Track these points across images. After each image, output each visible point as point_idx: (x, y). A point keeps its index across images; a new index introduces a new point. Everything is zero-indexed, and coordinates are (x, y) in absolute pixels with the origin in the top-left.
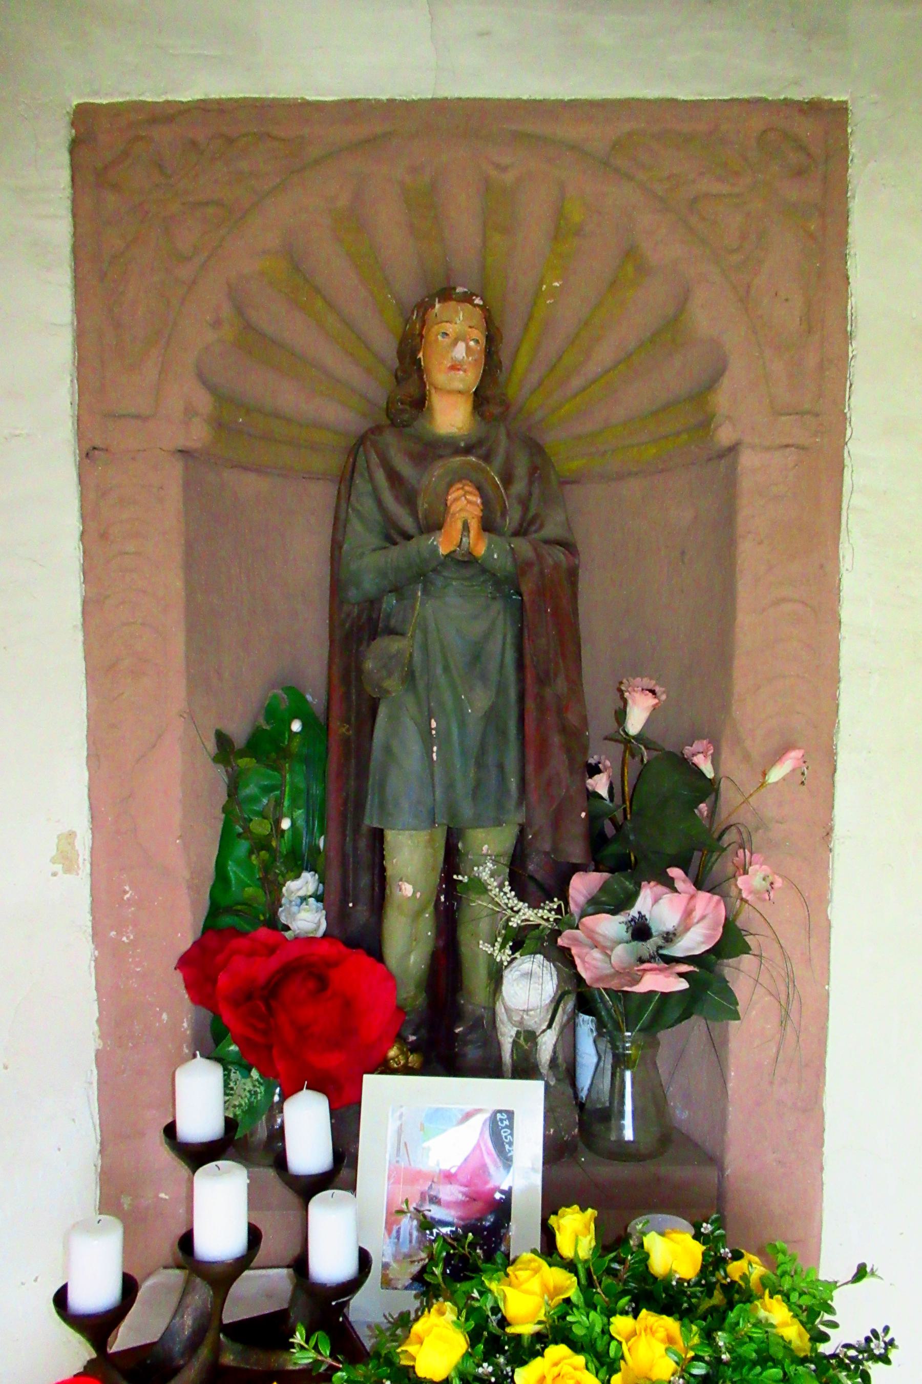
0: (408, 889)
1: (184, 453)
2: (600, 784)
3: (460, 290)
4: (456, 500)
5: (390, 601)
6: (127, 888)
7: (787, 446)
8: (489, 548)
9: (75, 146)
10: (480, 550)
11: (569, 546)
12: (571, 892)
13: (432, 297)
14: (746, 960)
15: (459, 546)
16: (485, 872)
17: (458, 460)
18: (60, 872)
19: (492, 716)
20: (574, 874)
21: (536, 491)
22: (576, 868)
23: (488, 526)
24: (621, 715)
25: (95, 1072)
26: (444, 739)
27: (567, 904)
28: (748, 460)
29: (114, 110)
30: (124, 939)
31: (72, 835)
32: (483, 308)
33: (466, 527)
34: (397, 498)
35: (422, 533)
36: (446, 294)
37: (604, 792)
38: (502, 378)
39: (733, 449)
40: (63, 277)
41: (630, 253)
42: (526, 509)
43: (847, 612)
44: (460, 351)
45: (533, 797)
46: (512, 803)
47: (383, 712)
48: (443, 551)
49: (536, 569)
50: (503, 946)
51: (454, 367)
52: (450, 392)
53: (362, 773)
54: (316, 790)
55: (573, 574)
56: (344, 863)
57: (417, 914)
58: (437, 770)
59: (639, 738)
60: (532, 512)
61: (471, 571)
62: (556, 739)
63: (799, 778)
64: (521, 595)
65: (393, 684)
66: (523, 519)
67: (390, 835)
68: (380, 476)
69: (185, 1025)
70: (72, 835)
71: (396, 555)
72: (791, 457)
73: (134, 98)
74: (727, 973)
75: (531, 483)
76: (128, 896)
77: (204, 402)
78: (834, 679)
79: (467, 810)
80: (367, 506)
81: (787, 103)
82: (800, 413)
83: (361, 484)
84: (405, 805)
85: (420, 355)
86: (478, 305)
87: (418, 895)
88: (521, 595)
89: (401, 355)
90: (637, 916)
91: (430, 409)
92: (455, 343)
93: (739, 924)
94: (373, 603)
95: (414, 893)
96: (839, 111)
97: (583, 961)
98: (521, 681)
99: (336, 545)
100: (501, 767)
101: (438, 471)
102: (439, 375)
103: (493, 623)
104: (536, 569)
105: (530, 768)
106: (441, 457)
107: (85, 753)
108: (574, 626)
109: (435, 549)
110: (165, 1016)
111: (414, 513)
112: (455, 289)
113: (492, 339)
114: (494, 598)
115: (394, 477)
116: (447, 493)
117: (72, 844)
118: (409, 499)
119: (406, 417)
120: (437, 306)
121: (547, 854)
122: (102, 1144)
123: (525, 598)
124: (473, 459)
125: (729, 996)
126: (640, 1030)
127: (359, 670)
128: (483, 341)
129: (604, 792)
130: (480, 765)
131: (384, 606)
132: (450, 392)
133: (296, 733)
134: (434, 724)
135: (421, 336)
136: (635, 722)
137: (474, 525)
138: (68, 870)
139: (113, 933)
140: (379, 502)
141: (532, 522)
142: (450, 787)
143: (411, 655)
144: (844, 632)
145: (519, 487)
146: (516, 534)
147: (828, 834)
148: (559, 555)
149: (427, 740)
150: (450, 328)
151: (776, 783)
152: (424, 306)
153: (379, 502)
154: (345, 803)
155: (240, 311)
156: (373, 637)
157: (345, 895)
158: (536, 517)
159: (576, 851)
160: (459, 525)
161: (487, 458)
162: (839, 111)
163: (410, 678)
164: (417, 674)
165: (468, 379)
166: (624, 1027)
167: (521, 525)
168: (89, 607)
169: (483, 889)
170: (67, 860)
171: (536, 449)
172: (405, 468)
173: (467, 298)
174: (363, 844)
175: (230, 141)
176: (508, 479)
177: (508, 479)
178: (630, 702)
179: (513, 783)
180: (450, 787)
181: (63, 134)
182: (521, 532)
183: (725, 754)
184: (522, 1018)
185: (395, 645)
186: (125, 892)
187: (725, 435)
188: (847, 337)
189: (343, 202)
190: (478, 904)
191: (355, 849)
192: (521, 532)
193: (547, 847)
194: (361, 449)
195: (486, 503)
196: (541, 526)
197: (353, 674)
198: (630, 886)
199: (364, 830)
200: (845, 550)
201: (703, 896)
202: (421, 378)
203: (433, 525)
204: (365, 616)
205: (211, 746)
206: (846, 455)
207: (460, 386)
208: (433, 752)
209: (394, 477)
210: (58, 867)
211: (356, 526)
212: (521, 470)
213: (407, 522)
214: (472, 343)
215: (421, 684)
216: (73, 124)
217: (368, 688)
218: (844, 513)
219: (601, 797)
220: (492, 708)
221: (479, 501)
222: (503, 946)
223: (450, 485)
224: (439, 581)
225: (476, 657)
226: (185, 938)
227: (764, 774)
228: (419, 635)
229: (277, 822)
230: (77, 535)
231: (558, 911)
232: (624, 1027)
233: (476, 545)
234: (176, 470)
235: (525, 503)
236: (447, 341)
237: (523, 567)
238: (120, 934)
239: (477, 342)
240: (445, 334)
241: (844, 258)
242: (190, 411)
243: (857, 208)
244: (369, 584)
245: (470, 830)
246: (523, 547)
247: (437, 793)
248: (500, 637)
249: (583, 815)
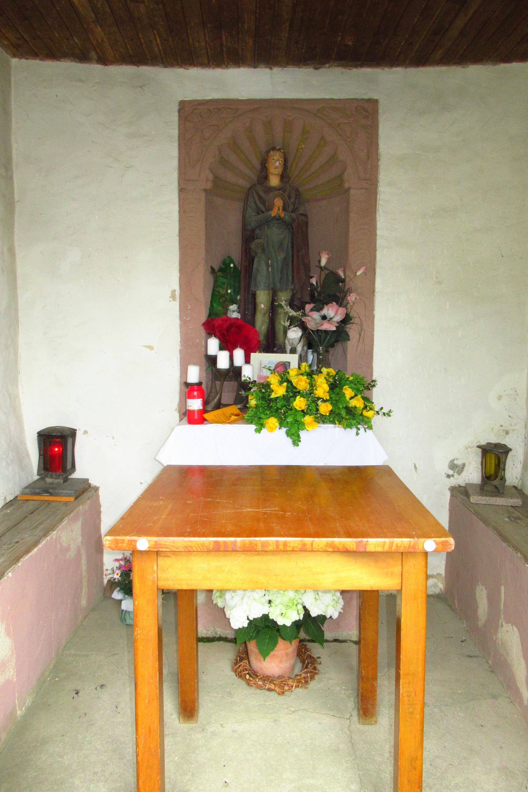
0: (263, 306)
1: (205, 190)
2: (314, 281)
3: (277, 148)
4: (276, 202)
5: (258, 231)
6: (189, 306)
7: (362, 188)
8: (284, 215)
9: (179, 111)
10: (282, 215)
11: (306, 216)
12: (306, 309)
13: (271, 149)
14: (354, 326)
15: (277, 214)
16: (283, 303)
17: (277, 192)
18: (172, 301)
19: (285, 259)
20: (338, 618)
21: (297, 202)
22: (307, 303)
23: (284, 209)
24: (319, 261)
25: (179, 355)
26: (272, 266)
27: (304, 311)
28: (352, 192)
29: (190, 102)
30: (188, 319)
31: (175, 291)
32: (284, 152)
33: (279, 209)
34: (260, 203)
35: (267, 211)
36: (274, 149)
37: (315, 283)
38: (288, 171)
39: (349, 189)
40: (176, 144)
41: (323, 138)
42: (294, 206)
43: (379, 232)
44: (277, 164)
45: (296, 281)
46: (290, 284)
47: (256, 260)
48: (273, 215)
49: (297, 221)
50: (287, 321)
51: (276, 168)
52: (274, 174)
53: (250, 276)
54: (237, 284)
55: (306, 223)
56: (245, 302)
57: (265, 314)
58: (271, 274)
59: (325, 267)
60: (296, 206)
61: (279, 221)
62: (302, 267)
63: (365, 273)
64: (293, 229)
65: (259, 251)
66: (294, 208)
67: (258, 292)
68: (256, 197)
69: (203, 342)
70: (175, 291)
71: (261, 216)
72: (363, 191)
73: (195, 99)
74: (347, 330)
75: (296, 199)
76: (189, 308)
77: (211, 177)
78: (375, 250)
79: (278, 285)
80: (253, 205)
81: (363, 99)
82: (366, 180)
83: (251, 200)
84: (262, 283)
85: (267, 165)
86: (282, 152)
87: (265, 308)
88: (293, 229)
89: (261, 164)
90: (365, 543)
91: (269, 179)
92: (276, 161)
93: (351, 315)
94: (253, 231)
95: (264, 307)
96: (376, 101)
97: (309, 324)
98: (293, 251)
99: (244, 217)
100: (287, 274)
101: (271, 195)
102: (272, 170)
103: (285, 236)
104: (297, 221)
105: (295, 274)
106: (272, 192)
107: (178, 269)
108: (307, 237)
109: (271, 215)
110: (198, 340)
111: (265, 206)
112: (276, 147)
113: (286, 161)
114: (286, 229)
115: (260, 197)
116: (274, 200)
117: (175, 293)
118: (263, 202)
119: (262, 181)
120: (272, 152)
121: (299, 299)
122: (181, 375)
123: (294, 230)
124: (281, 192)
125: (348, 336)
126: (325, 346)
127: (250, 249)
128: (283, 161)
129: (315, 283)
130: (282, 272)
131: (256, 233)
132: (274, 174)
133: (232, 267)
134: (270, 262)
135: (267, 160)
136: (323, 262)
137: (281, 208)
138: (174, 300)
139: (185, 318)
140: (256, 203)
141: (296, 209)
142: (274, 278)
143: (264, 244)
144: (378, 237)
145: (292, 200)
146: (292, 212)
147: (374, 291)
148: (303, 217)
149: (268, 266)
150: (275, 158)
151: (359, 275)
152: (268, 152)
153: (256, 203)
154: (246, 285)
155: (220, 152)
156: (253, 240)
157: (245, 310)
158: (297, 207)
159: (307, 298)
160: (277, 208)
161: (284, 192)
162: (376, 101)
163: (263, 250)
164: (265, 249)
165: (279, 171)
166: (320, 345)
167: (293, 210)
168: (181, 230)
169: (282, 307)
170: (173, 297)
171: (297, 190)
172: (262, 194)
173: (279, 150)
174: (250, 296)
175: (219, 109)
176: (290, 198)
177: (290, 198)
178: (321, 256)
179: (290, 278)
180: (274, 278)
181: (176, 108)
182: (293, 211)
183: (347, 271)
184: (292, 342)
185: (259, 241)
186: (188, 307)
187: (346, 185)
188: (378, 160)
189: (248, 125)
190: (280, 310)
191: (248, 297)
192: (293, 211)
193: (299, 297)
194: (250, 191)
195: (284, 203)
196: (298, 211)
197: (248, 250)
198: (321, 306)
199: (250, 292)
200: (378, 215)
201: (341, 308)
202: (267, 171)
203: (270, 209)
204: (251, 235)
205: (210, 269)
206: (378, 190)
207: (277, 173)
208: (269, 269)
209: (260, 197)
210: (171, 299)
211: (249, 210)
212: (293, 195)
213: (263, 209)
214: (280, 162)
215: (266, 252)
216: (179, 105)
217: (252, 253)
218: (377, 206)
219: (314, 285)
220: (285, 257)
221: (282, 202)
222: (287, 321)
223: (275, 198)
224: (272, 225)
225: (281, 244)
226: (204, 319)
227: (356, 273)
228: (266, 239)
229: (227, 291)
230: (178, 211)
231: (302, 313)
232: (320, 345)
233: (281, 214)
234: (203, 195)
235: (294, 204)
236: (274, 161)
237: (293, 220)
238: (186, 318)
239: (282, 161)
240: (273, 159)
241: (377, 139)
242: (207, 180)
243: (380, 126)
244: (253, 224)
245: (279, 292)
246: (294, 215)
247: (271, 280)
248: (287, 240)
249: (309, 289)
